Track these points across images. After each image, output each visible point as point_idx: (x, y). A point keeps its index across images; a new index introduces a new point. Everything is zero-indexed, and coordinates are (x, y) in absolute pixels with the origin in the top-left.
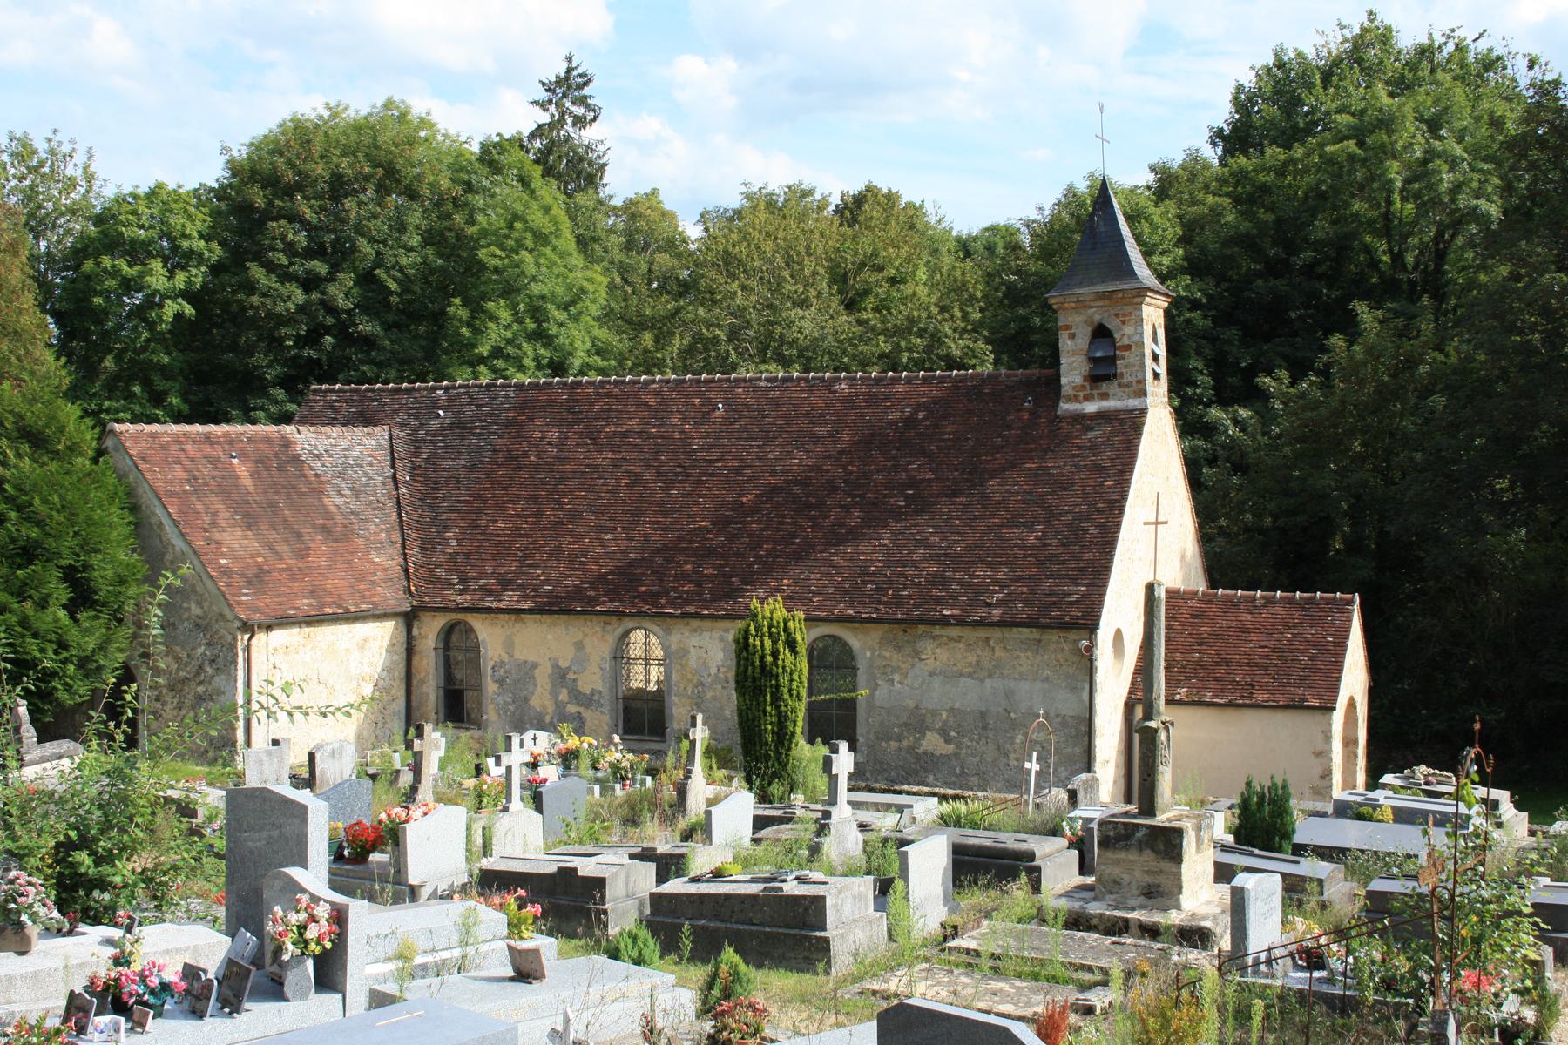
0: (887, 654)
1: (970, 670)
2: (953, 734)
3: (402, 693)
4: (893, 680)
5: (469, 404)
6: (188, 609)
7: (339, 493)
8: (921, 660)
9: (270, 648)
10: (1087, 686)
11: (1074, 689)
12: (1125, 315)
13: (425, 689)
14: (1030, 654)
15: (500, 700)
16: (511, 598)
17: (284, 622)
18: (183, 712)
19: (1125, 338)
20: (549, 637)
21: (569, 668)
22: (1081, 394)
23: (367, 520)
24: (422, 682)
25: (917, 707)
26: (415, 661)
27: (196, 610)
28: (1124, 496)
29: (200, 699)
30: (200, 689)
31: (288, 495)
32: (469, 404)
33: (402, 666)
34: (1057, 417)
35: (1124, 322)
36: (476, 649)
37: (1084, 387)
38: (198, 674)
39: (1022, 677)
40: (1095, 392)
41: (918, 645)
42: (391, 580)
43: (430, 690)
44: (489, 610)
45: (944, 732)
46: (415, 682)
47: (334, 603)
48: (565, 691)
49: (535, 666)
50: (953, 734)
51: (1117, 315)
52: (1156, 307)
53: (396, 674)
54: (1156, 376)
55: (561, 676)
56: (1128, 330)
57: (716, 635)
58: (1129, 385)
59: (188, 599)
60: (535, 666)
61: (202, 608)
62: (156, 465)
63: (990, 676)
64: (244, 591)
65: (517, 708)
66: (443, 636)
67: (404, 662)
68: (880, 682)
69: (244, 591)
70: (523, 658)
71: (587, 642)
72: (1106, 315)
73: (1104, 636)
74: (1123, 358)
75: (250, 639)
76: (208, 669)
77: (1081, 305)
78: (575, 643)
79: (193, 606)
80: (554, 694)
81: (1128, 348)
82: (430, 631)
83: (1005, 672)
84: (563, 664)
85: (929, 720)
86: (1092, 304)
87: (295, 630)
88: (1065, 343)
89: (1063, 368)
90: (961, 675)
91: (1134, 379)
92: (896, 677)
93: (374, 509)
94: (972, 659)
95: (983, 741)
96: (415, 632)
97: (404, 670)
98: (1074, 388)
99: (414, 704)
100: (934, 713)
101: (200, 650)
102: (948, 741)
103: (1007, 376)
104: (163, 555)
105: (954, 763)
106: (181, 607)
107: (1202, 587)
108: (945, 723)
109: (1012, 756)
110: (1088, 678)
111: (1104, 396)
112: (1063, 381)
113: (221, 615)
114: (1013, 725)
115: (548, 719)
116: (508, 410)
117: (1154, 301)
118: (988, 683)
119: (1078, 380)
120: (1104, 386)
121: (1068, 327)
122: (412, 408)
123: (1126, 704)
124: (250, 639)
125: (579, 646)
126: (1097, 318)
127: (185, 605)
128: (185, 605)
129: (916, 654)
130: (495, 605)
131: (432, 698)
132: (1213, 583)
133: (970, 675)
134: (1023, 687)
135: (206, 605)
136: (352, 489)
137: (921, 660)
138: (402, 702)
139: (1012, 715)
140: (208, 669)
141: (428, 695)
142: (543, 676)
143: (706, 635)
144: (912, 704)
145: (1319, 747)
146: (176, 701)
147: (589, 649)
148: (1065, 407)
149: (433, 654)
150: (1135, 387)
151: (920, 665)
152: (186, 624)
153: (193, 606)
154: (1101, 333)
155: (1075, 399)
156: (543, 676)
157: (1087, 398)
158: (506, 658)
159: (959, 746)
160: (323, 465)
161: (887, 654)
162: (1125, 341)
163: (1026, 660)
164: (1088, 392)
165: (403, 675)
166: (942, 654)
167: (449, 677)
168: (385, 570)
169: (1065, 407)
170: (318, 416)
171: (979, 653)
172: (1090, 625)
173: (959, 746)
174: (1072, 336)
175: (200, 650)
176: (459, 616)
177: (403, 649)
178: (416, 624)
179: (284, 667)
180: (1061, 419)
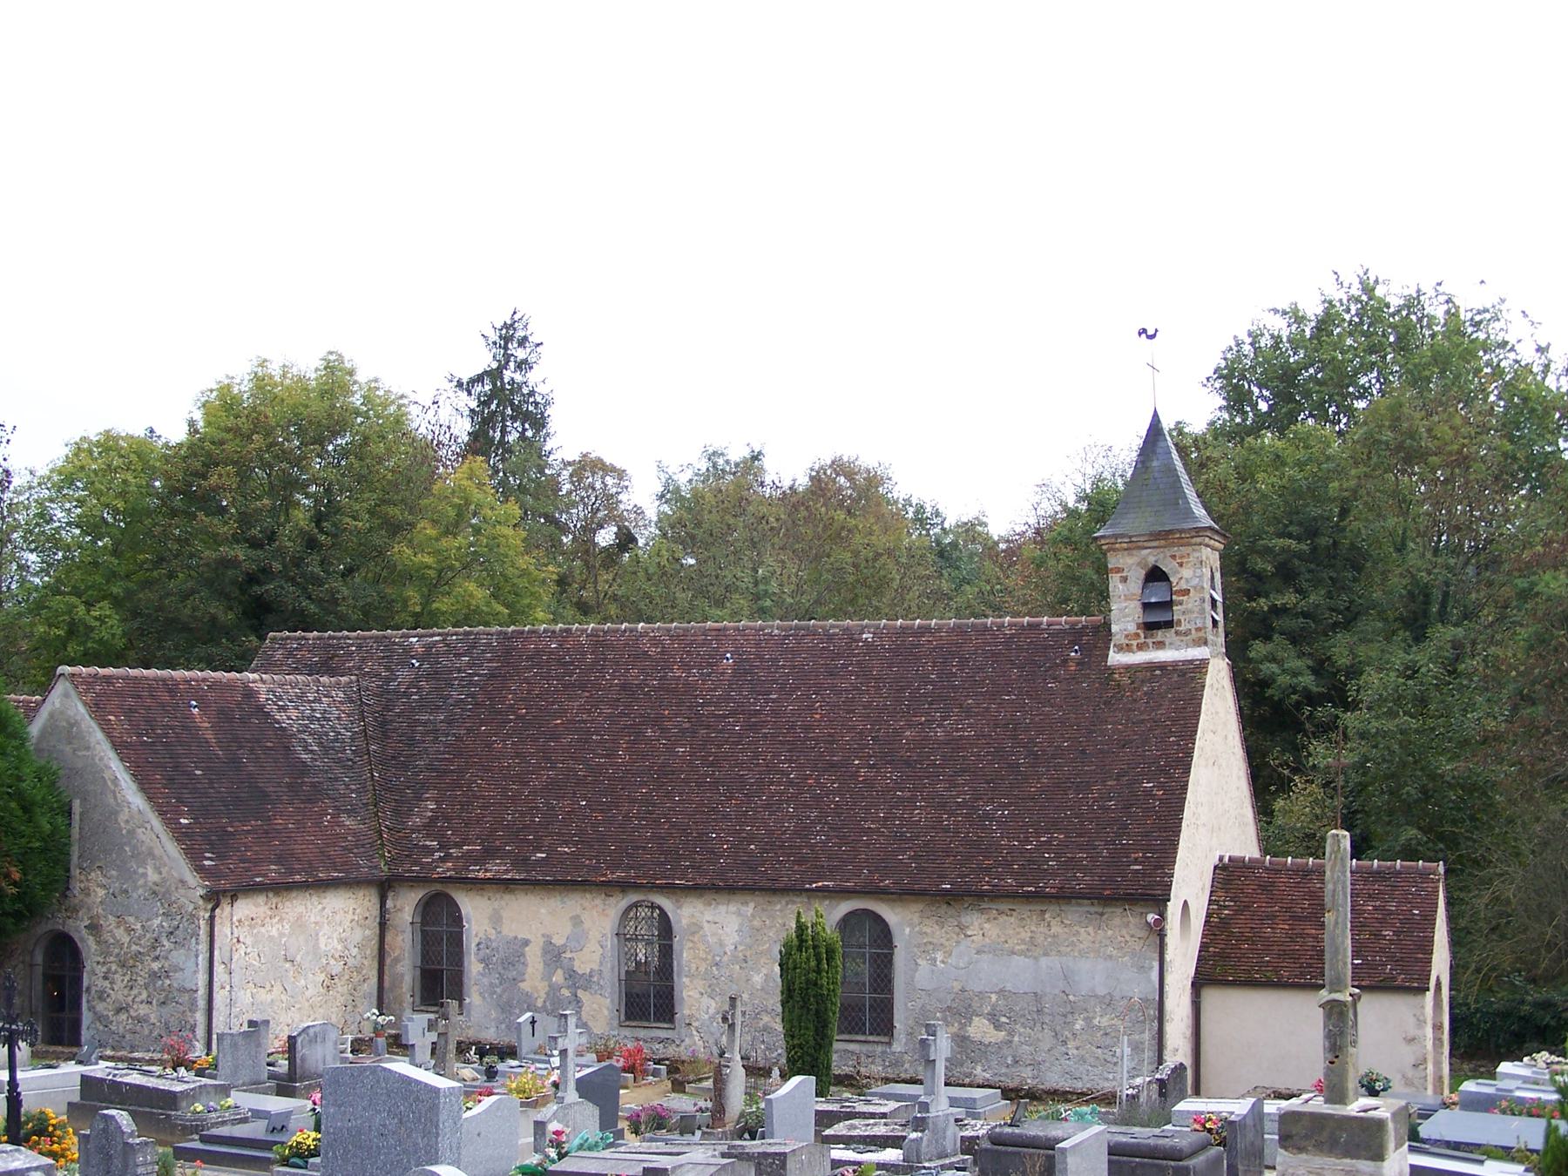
0: (929, 930)
1: (1023, 947)
2: (1004, 1019)
3: (374, 974)
4: (935, 960)
5: (448, 653)
6: (145, 875)
7: (306, 749)
8: (967, 936)
9: (235, 919)
10: (1156, 965)
11: (1142, 969)
12: (1182, 557)
13: (400, 968)
14: (1090, 929)
15: (485, 981)
16: (495, 868)
17: (252, 889)
18: (135, 992)
19: (1183, 581)
20: (543, 911)
21: (565, 945)
22: (1134, 643)
23: (336, 779)
24: (397, 960)
25: (963, 990)
26: (388, 938)
27: (153, 876)
28: (1189, 754)
29: (154, 976)
30: (156, 966)
31: (252, 750)
32: (448, 653)
33: (375, 943)
34: (1109, 668)
35: (1181, 565)
36: (457, 919)
37: (1137, 635)
38: (154, 948)
39: (1083, 954)
40: (1150, 641)
41: (963, 920)
42: (363, 846)
43: (406, 969)
44: (476, 881)
45: (993, 1018)
46: (388, 961)
47: (303, 869)
48: (560, 972)
49: (526, 943)
50: (1004, 1019)
51: (1173, 557)
52: (1213, 549)
53: (368, 952)
54: (1215, 622)
55: (554, 956)
56: (1186, 573)
57: (732, 908)
58: (1187, 633)
59: (143, 864)
60: (526, 943)
61: (160, 873)
62: (111, 713)
63: (1046, 954)
64: (208, 855)
65: (504, 991)
66: (420, 909)
67: (377, 938)
68: (919, 961)
69: (208, 855)
70: (512, 935)
71: (585, 916)
72: (1162, 556)
73: (1173, 909)
74: (1181, 603)
75: (213, 910)
76: (165, 943)
77: (1133, 546)
78: (571, 918)
79: (150, 871)
80: (547, 976)
81: (1186, 592)
82: (406, 905)
83: (1062, 949)
84: (558, 941)
85: (975, 1005)
86: (1146, 544)
87: (261, 899)
88: (1116, 585)
89: (1114, 615)
90: (1013, 953)
91: (1192, 627)
92: (939, 956)
93: (343, 767)
94: (1026, 935)
95: (1038, 1026)
96: (389, 904)
97: (376, 946)
98: (1127, 636)
99: (387, 984)
100: (981, 995)
101: (157, 922)
102: (998, 1027)
103: (1049, 625)
104: (116, 813)
105: (1005, 1051)
106: (135, 872)
107: (1256, 854)
108: (994, 1007)
109: (1071, 1044)
110: (1156, 956)
111: (1160, 645)
112: (1114, 628)
113: (183, 882)
114: (1073, 1010)
115: (539, 1003)
116: (490, 661)
117: (1212, 542)
118: (1044, 961)
119: (1132, 628)
120: (1160, 635)
121: (1119, 570)
122: (383, 658)
123: (1193, 984)
124: (213, 910)
125: (577, 921)
126: (1151, 560)
127: (141, 870)
128: (141, 870)
129: (962, 928)
130: (481, 875)
131: (408, 979)
132: (1265, 851)
133: (1022, 953)
134: (1084, 966)
135: (164, 870)
136: (320, 744)
137: (967, 936)
138: (374, 980)
139: (1071, 997)
140: (165, 943)
141: (402, 975)
142: (533, 955)
143: (723, 908)
144: (957, 986)
145: (1412, 1032)
146: (127, 978)
147: (587, 924)
148: (1115, 658)
149: (409, 929)
150: (1194, 634)
151: (966, 942)
152: (140, 891)
153: (150, 871)
154: (1156, 575)
155: (1127, 648)
156: (533, 955)
157: (1140, 647)
158: (493, 934)
159: (1011, 1033)
160: (289, 718)
161: (929, 930)
162: (1183, 585)
163: (1087, 935)
164: (1142, 640)
165: (376, 952)
166: (992, 930)
167: (426, 955)
168: (355, 834)
169: (1115, 658)
170: (276, 665)
171: (1033, 928)
172: (1159, 900)
173: (1011, 1033)
174: (1124, 580)
175: (157, 922)
176: (438, 887)
177: (376, 924)
178: (390, 894)
179: (249, 941)
180: (1111, 670)
